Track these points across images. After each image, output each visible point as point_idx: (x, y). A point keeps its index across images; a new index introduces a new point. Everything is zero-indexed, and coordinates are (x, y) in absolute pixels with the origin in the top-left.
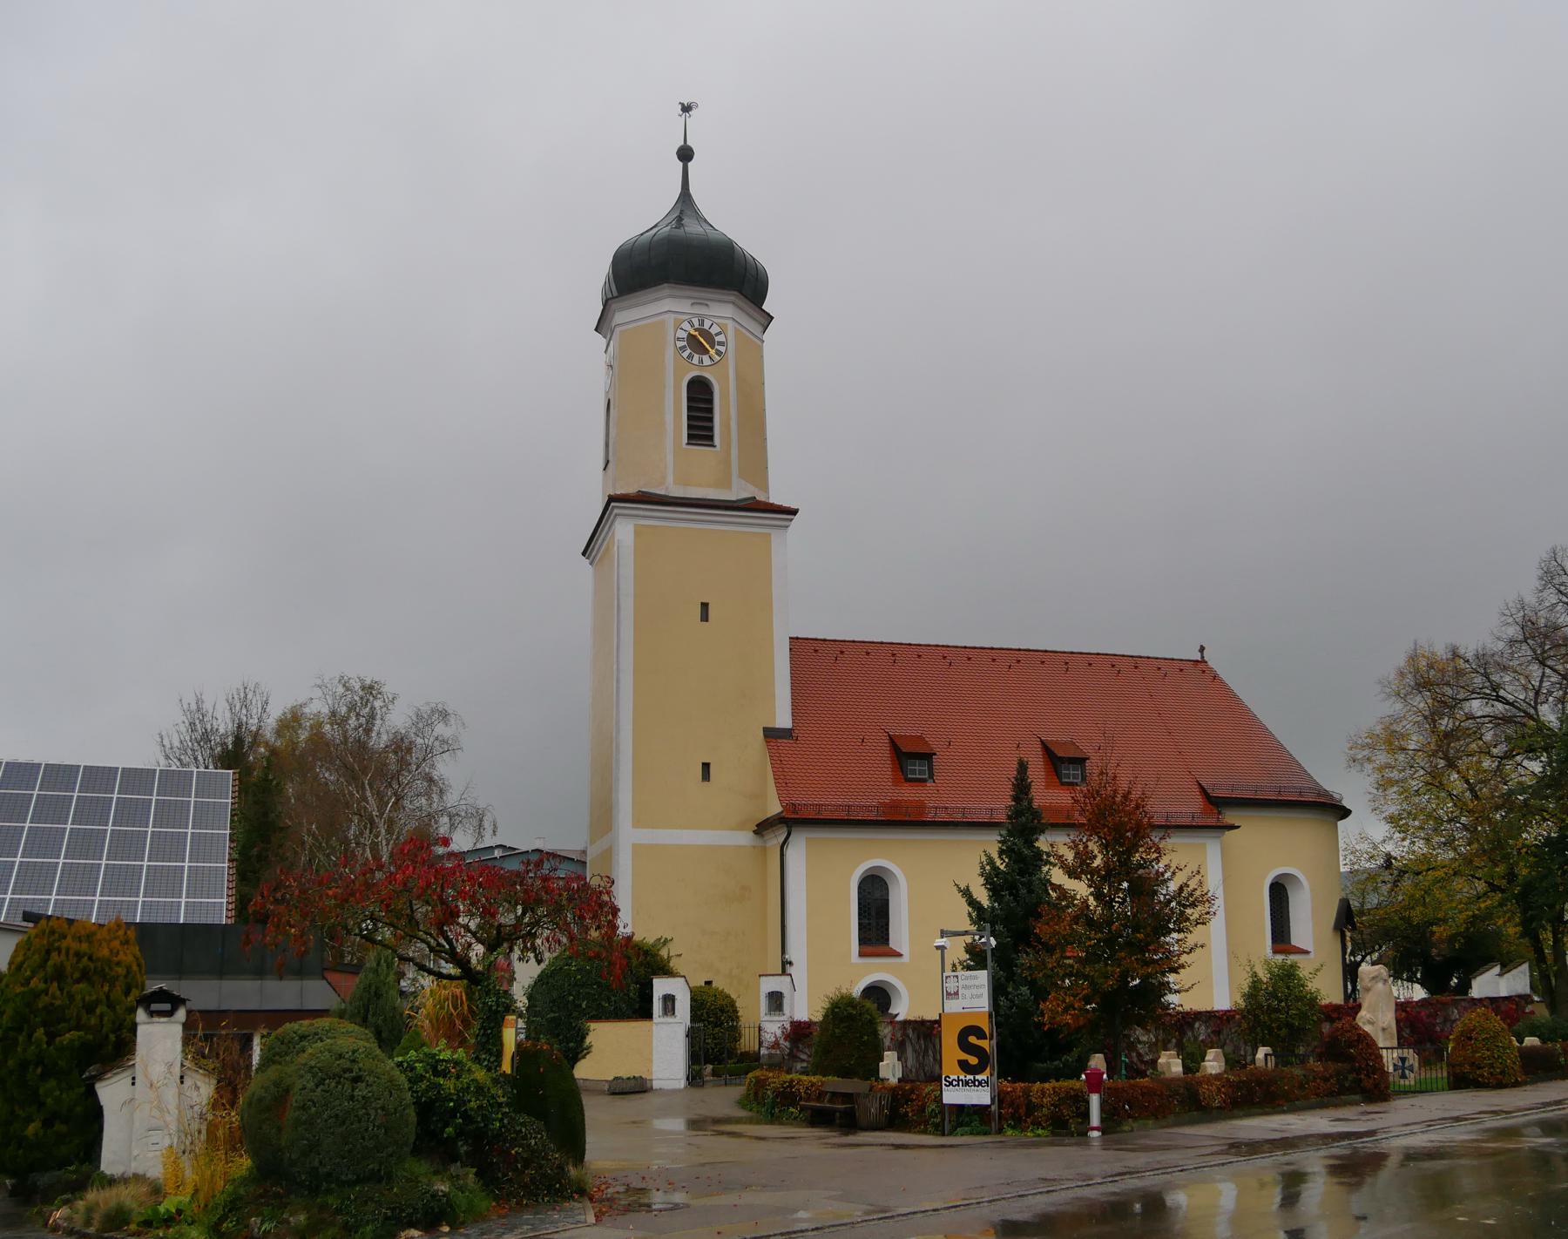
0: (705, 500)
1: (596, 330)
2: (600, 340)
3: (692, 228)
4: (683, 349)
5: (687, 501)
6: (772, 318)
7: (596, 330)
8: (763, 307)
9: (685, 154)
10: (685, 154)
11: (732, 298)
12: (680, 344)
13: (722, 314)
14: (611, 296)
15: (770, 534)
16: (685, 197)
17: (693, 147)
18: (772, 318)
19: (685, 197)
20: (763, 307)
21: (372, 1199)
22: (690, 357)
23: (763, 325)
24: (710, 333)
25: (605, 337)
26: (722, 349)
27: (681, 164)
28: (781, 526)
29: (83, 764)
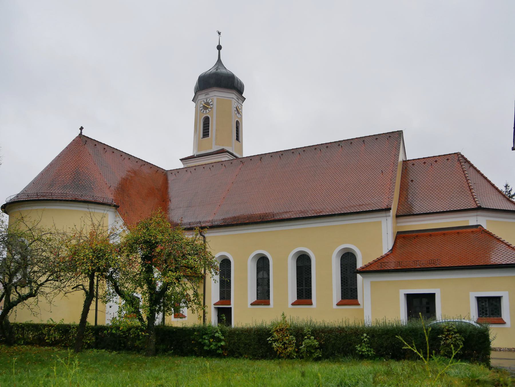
0: (201, 154)
1: (192, 101)
2: (194, 104)
3: (221, 70)
4: (202, 110)
5: (205, 155)
6: (245, 99)
7: (192, 101)
8: (242, 95)
9: (219, 48)
10: (219, 48)
11: (214, 89)
12: (201, 109)
13: (231, 96)
14: (197, 91)
15: (381, 221)
16: (219, 60)
17: (221, 45)
18: (245, 99)
19: (219, 60)
20: (242, 95)
21: (137, 280)
22: (203, 112)
23: (242, 101)
24: (210, 104)
25: (195, 103)
26: (205, 112)
27: (218, 51)
28: (197, 161)
29: (232, 306)
